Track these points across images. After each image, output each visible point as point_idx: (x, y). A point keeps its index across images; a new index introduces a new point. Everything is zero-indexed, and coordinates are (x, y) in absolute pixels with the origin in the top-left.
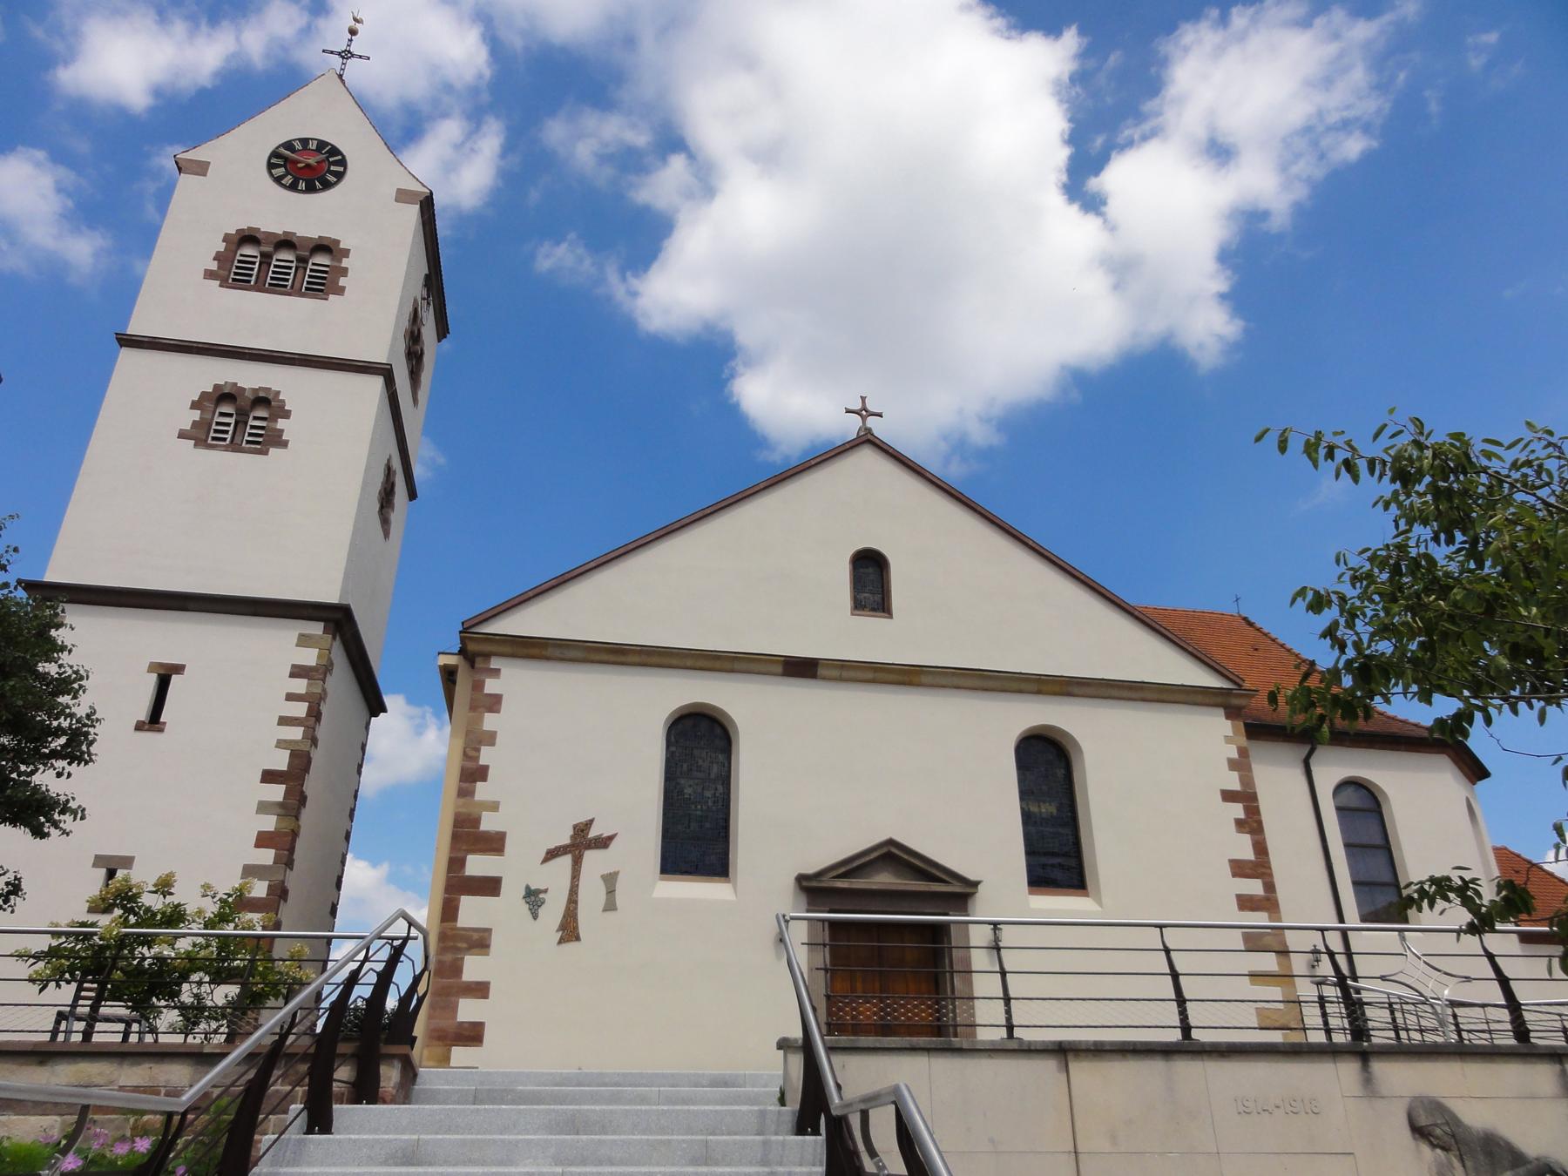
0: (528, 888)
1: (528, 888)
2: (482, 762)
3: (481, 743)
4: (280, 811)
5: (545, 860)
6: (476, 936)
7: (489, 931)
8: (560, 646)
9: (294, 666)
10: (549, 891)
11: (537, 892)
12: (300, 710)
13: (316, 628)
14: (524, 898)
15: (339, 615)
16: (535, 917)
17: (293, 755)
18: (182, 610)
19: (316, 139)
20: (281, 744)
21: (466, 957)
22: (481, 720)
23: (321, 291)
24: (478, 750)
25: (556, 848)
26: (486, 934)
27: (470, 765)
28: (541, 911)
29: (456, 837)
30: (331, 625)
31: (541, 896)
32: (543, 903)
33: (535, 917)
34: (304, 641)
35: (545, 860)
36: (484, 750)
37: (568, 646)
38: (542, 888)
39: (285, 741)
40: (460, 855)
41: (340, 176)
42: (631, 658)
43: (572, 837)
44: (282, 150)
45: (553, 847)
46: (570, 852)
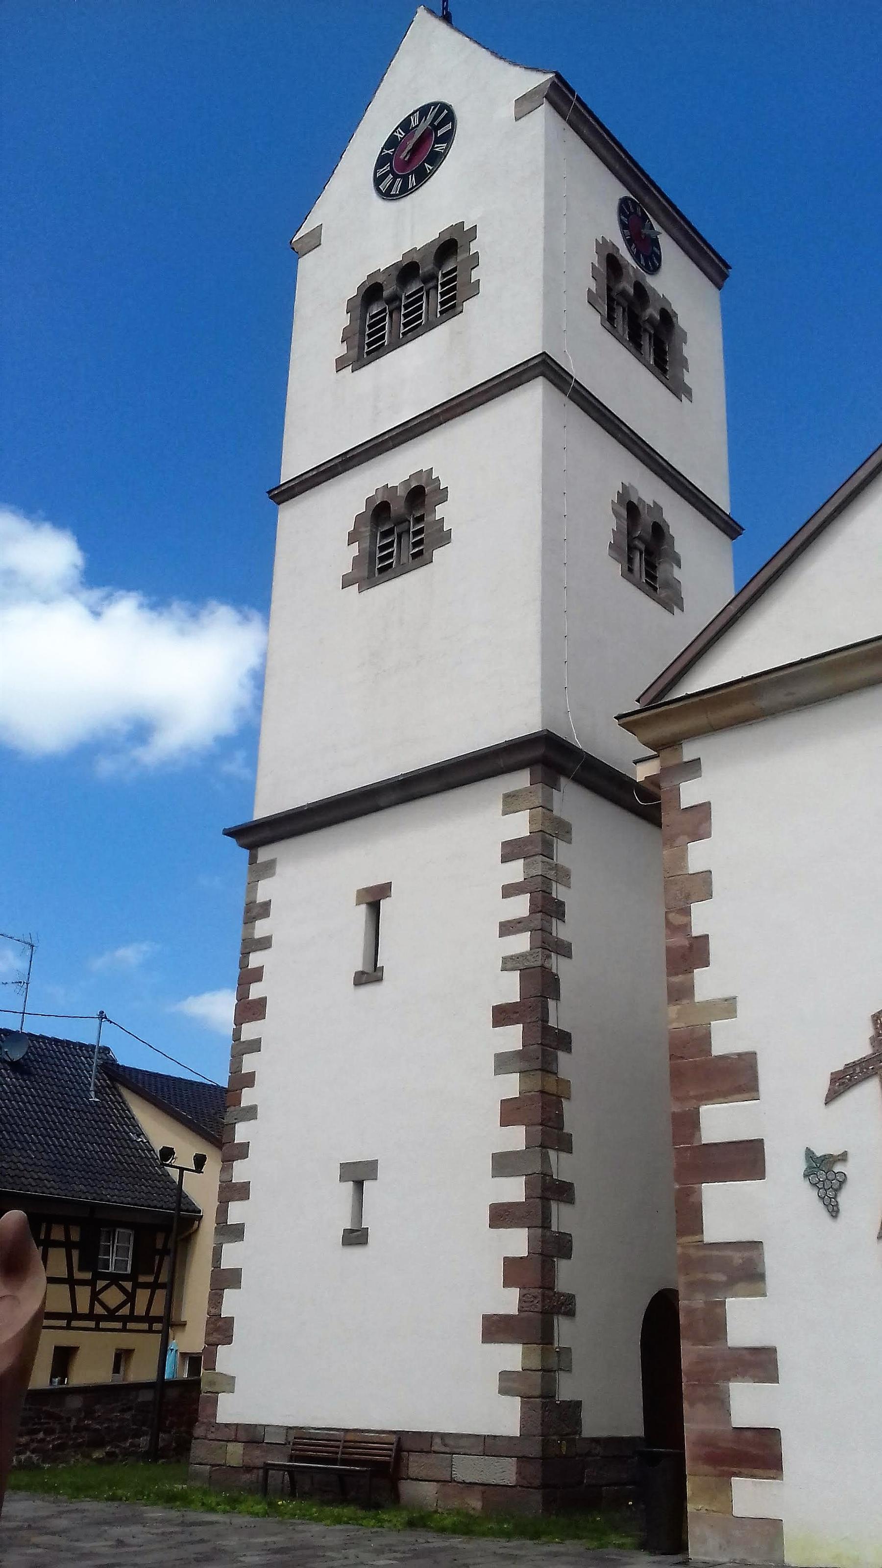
0: (809, 1154)
1: (809, 1154)
2: (696, 931)
3: (689, 898)
4: (525, 1066)
5: (832, 1097)
6: (737, 1257)
7: (756, 1245)
8: (779, 682)
9: (505, 844)
10: (850, 1158)
11: (828, 1161)
12: (520, 907)
13: (521, 780)
14: (806, 1176)
15: (539, 752)
16: (834, 1211)
17: (526, 975)
18: (493, 776)
19: (397, 128)
20: (509, 964)
21: (729, 1301)
22: (682, 857)
23: (454, 306)
24: (687, 912)
25: (847, 1067)
26: (754, 1254)
27: (680, 941)
28: (843, 1199)
29: (677, 1075)
30: (539, 769)
31: (838, 1168)
32: (842, 1183)
33: (834, 1211)
34: (511, 802)
35: (832, 1097)
36: (697, 908)
37: (794, 677)
38: (836, 1151)
39: (511, 958)
40: (688, 1106)
41: (378, 181)
42: (804, 690)
43: (873, 1040)
44: (449, 126)
45: (841, 1067)
46: (874, 1073)
